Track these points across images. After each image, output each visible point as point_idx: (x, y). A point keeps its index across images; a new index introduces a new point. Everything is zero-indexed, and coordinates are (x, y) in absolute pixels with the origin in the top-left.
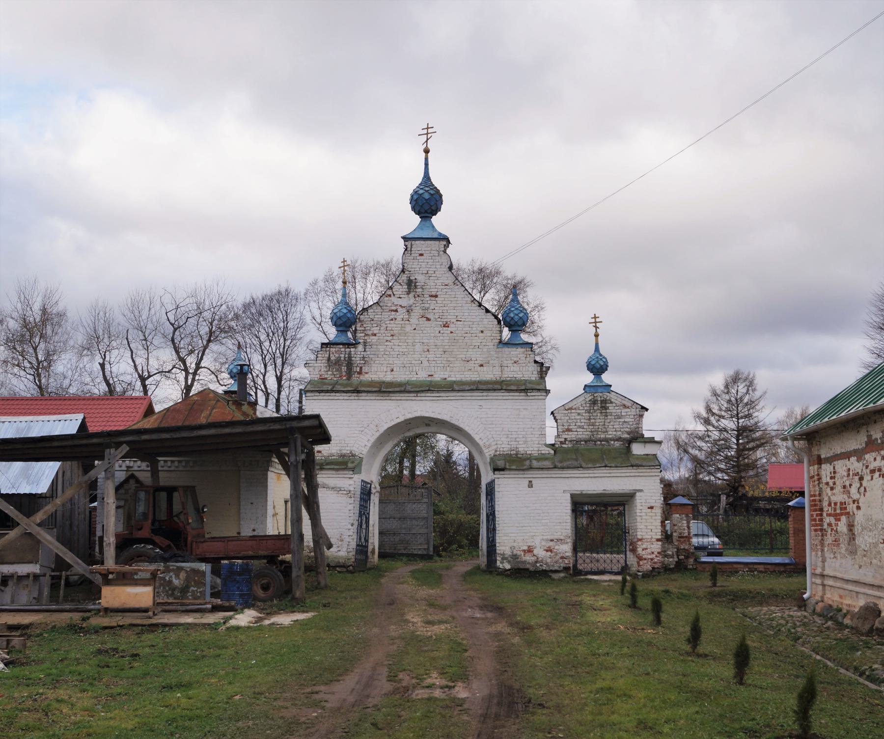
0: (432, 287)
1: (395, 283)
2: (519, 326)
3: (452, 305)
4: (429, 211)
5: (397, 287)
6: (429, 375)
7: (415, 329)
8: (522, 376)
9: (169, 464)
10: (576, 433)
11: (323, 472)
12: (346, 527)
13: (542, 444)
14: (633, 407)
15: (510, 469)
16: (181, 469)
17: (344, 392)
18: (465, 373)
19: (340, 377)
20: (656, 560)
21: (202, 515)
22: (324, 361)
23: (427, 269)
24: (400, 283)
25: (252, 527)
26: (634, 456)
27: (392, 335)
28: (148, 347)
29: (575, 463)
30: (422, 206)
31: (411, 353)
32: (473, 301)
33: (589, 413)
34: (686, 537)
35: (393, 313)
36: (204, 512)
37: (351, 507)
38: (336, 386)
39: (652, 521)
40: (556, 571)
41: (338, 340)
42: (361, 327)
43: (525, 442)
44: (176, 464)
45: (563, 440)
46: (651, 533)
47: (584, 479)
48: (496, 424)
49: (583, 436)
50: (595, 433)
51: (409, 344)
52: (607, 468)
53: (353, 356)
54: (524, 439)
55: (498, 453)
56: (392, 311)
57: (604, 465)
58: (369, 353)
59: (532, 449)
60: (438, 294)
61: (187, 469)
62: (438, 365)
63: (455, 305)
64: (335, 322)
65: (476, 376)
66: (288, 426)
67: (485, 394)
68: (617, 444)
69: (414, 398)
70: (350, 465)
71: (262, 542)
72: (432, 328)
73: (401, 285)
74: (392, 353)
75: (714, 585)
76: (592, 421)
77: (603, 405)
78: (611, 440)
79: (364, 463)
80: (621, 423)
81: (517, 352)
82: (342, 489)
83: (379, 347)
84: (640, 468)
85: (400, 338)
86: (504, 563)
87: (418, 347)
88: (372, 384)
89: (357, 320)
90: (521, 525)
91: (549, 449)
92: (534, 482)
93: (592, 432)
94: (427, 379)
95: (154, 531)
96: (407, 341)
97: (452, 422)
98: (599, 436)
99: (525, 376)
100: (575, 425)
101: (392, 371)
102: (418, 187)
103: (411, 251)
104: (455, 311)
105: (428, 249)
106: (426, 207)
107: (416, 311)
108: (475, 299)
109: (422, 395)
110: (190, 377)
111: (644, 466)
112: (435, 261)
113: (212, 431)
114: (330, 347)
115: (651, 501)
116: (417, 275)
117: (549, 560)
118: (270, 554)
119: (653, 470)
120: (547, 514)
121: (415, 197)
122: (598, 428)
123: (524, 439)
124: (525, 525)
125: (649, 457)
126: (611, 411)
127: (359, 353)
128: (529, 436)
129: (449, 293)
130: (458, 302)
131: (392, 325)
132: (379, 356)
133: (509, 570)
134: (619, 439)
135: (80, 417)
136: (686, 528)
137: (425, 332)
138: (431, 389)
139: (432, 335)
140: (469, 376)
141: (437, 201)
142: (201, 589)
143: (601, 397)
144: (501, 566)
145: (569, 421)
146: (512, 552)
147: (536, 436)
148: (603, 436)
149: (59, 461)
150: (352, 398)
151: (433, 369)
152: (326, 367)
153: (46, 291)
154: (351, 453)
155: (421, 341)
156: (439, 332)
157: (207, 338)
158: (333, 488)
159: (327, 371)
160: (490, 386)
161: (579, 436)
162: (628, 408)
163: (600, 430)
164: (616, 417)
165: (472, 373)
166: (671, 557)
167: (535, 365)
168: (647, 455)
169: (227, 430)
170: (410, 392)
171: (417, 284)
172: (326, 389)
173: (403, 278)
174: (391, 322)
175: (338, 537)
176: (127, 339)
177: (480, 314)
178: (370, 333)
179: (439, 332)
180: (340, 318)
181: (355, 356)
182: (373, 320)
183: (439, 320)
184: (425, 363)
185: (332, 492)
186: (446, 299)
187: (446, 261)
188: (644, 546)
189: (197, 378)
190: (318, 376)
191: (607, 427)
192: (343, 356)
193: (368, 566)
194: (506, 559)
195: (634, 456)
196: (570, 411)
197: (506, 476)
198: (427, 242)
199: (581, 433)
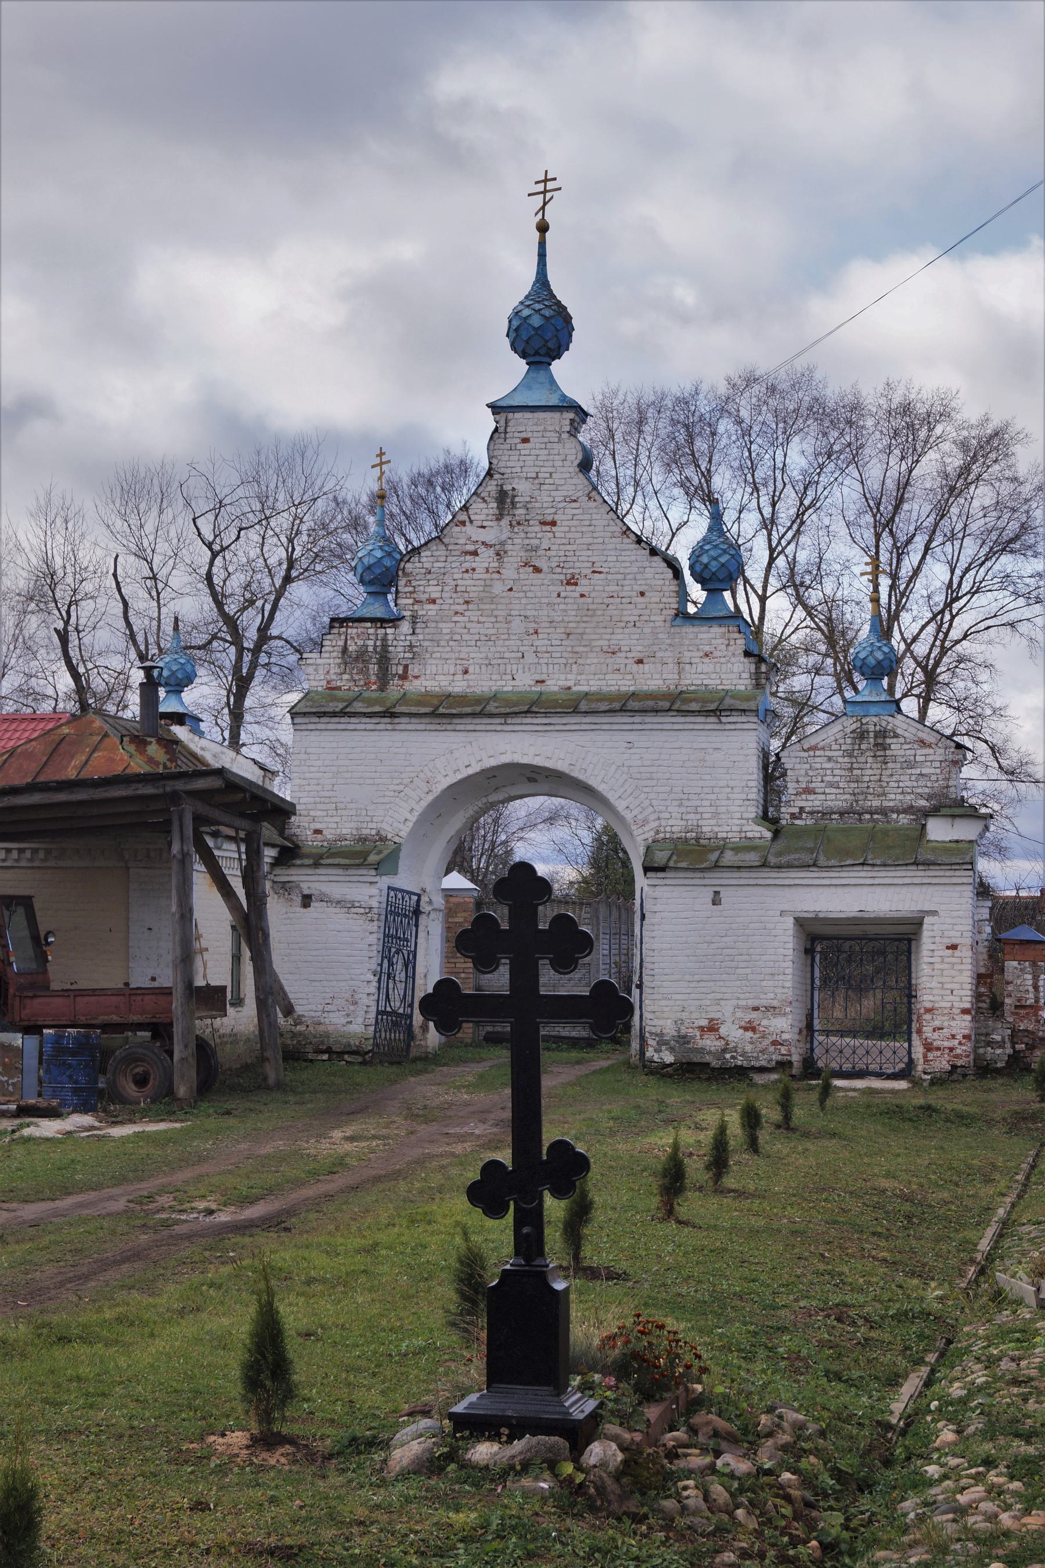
0: (545, 505)
1: (474, 498)
2: (721, 581)
3: (584, 541)
5: (477, 506)
6: (537, 682)
7: (511, 590)
8: (719, 682)
10: (823, 797)
12: (363, 978)
13: (748, 819)
14: (940, 745)
15: (676, 869)
16: (23, 864)
17: (365, 715)
18: (608, 677)
19: (366, 684)
20: (958, 1051)
21: (45, 948)
22: (335, 654)
23: (537, 469)
24: (483, 498)
25: (150, 973)
26: (930, 845)
27: (467, 602)
28: (158, 594)
29: (808, 858)
30: (527, 342)
31: (503, 637)
32: (625, 533)
33: (850, 756)
34: (1031, 1006)
35: (468, 557)
36: (48, 944)
38: (355, 704)
39: (953, 973)
40: (762, 1070)
41: (367, 613)
42: (406, 585)
43: (716, 815)
45: (797, 810)
46: (951, 998)
47: (821, 890)
48: (658, 780)
49: (837, 803)
50: (861, 797)
51: (500, 619)
52: (866, 868)
53: (390, 643)
54: (713, 809)
55: (662, 835)
56: (467, 553)
57: (861, 861)
58: (421, 637)
59: (728, 829)
60: (556, 517)
61: (34, 864)
62: (556, 661)
63: (590, 540)
64: (362, 576)
65: (629, 683)
66: (168, 789)
67: (637, 719)
68: (904, 820)
69: (499, 728)
70: (373, 858)
71: (133, 998)
73: (485, 501)
74: (465, 637)
76: (855, 772)
77: (880, 741)
78: (893, 812)
79: (402, 854)
80: (913, 778)
81: (713, 635)
82: (357, 904)
83: (440, 625)
84: (931, 867)
85: (482, 606)
86: (661, 1051)
87: (518, 626)
88: (424, 698)
89: (400, 573)
90: (696, 977)
91: (760, 828)
92: (724, 893)
93: (854, 794)
94: (533, 689)
96: (496, 613)
97: (572, 774)
98: (869, 803)
99: (724, 682)
100: (822, 781)
101: (466, 672)
102: (521, 303)
103: (506, 432)
104: (590, 553)
105: (541, 428)
106: (537, 344)
107: (514, 553)
109: (514, 721)
110: (247, 658)
111: (939, 864)
112: (552, 452)
113: (36, 798)
114: (347, 627)
115: (952, 933)
116: (516, 480)
117: (749, 1048)
118: (147, 1021)
119: (957, 873)
120: (748, 958)
121: (515, 323)
122: (868, 787)
123: (713, 809)
124: (705, 977)
125: (961, 845)
126: (895, 753)
127: (403, 638)
128: (724, 803)
129: (580, 517)
130: (595, 535)
131: (466, 582)
132: (442, 643)
133: (671, 1065)
134: (909, 810)
136: (1031, 989)
137: (529, 594)
138: (534, 709)
139: (544, 600)
140: (614, 682)
141: (557, 330)
142: (16, 1080)
143: (875, 725)
145: (811, 773)
146: (679, 1031)
147: (738, 803)
148: (876, 803)
151: (545, 670)
152: (339, 665)
155: (522, 613)
156: (559, 595)
157: (283, 573)
158: (339, 902)
159: (341, 674)
160: (650, 703)
161: (829, 803)
162: (930, 746)
163: (871, 790)
164: (905, 765)
165: (621, 677)
166: (1000, 1047)
167: (746, 660)
168: (957, 841)
169: (62, 797)
170: (491, 715)
171: (517, 499)
172: (331, 710)
173: (489, 488)
174: (466, 575)
175: (348, 995)
176: (115, 575)
177: (639, 558)
178: (423, 597)
179: (559, 595)
180: (369, 568)
181: (395, 643)
182: (430, 573)
183: (559, 570)
184: (530, 658)
185: (337, 910)
186: (573, 529)
187: (574, 451)
189: (263, 659)
190: (324, 683)
191: (885, 784)
192: (371, 643)
193: (414, 1052)
194: (666, 1043)
195: (930, 845)
196: (811, 753)
197: (668, 882)
198: (536, 415)
199: (833, 797)
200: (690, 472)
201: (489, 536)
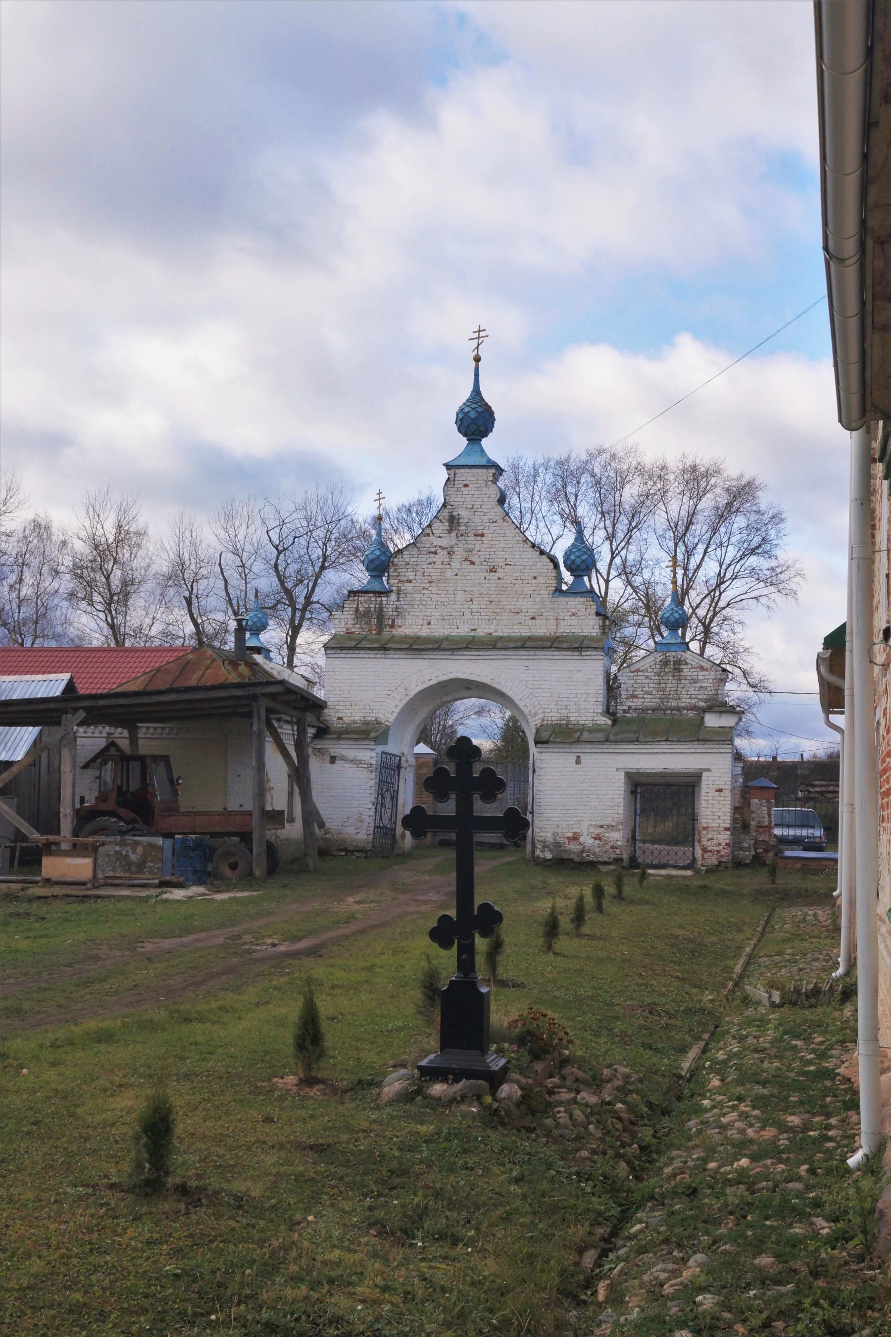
4: (477, 433)
5: (437, 525)
9: (152, 730)
11: (341, 742)
15: (554, 742)
16: (164, 736)
20: (723, 853)
30: (467, 427)
33: (659, 676)
34: (766, 826)
35: (431, 555)
36: (178, 784)
37: (373, 782)
38: (363, 642)
39: (720, 806)
41: (370, 588)
43: (578, 710)
44: (159, 731)
47: (641, 756)
54: (576, 707)
56: (430, 553)
66: (251, 692)
67: (531, 653)
68: (691, 714)
69: (449, 657)
72: (476, 574)
73: (441, 522)
75: (773, 882)
77: (677, 667)
87: (460, 596)
88: (404, 639)
90: (566, 808)
92: (583, 757)
95: (118, 804)
101: (429, 624)
106: (473, 428)
108: (527, 539)
110: (298, 614)
115: (719, 782)
117: (597, 850)
121: (460, 416)
123: (576, 707)
131: (430, 570)
133: (550, 860)
134: (694, 708)
135: (66, 676)
136: (766, 816)
144: (541, 856)
146: (555, 840)
148: (674, 704)
149: (34, 725)
150: (379, 656)
152: (353, 619)
153: (121, 503)
154: (376, 720)
158: (352, 761)
162: (707, 670)
168: (723, 727)
176: (220, 565)
178: (404, 579)
184: (468, 615)
188: (710, 836)
189: (308, 615)
193: (396, 851)
194: (547, 847)
197: (550, 750)
200: (564, 505)
201: (444, 542)
